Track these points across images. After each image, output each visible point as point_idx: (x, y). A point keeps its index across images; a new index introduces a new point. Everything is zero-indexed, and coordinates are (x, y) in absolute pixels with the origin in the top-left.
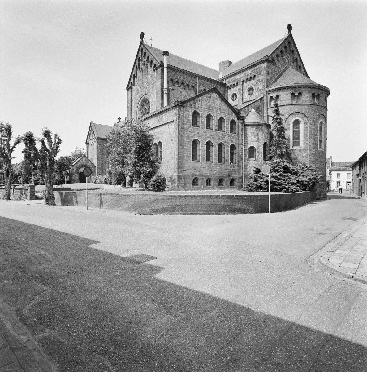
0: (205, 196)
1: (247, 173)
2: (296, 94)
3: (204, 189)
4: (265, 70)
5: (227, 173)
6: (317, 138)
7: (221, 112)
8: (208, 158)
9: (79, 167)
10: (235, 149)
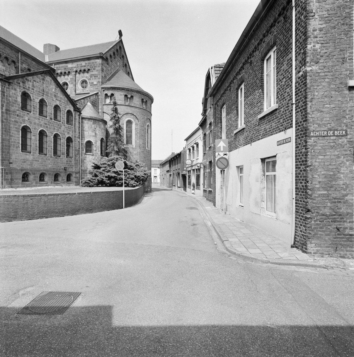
0: (58, 195)
1: (84, 168)
2: (129, 96)
3: (36, 186)
5: (63, 167)
6: (146, 139)
7: (56, 99)
8: (41, 150)
10: (72, 142)
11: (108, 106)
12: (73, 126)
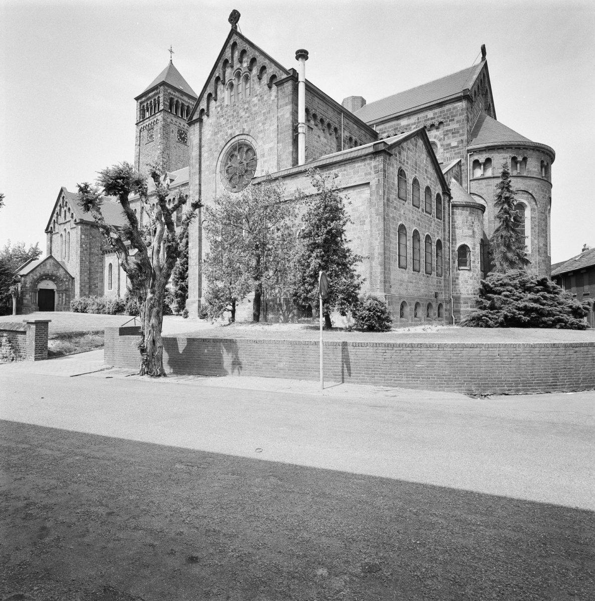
1: (457, 294)
2: (520, 159)
4: (463, 114)
9: (38, 279)
11: (480, 181)
12: (442, 221)
